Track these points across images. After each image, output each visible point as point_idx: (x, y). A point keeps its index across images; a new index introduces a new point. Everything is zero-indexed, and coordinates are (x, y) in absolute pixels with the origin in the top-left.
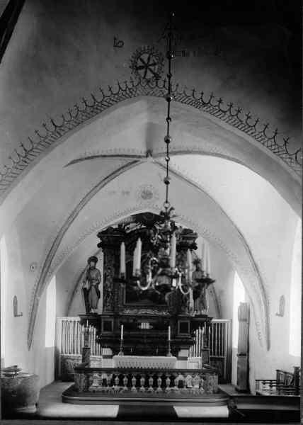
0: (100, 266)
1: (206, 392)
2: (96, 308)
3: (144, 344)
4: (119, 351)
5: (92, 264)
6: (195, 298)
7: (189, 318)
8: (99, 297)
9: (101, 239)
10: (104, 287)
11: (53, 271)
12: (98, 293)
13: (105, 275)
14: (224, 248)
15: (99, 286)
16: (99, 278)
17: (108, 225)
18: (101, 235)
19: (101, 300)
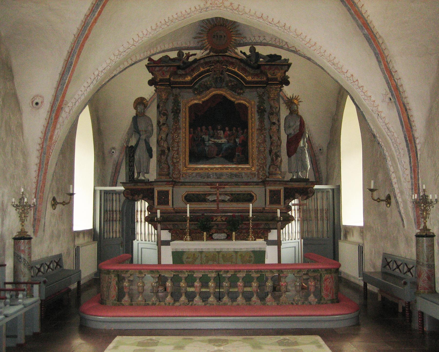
0: (152, 113)
1: (319, 302)
2: (148, 173)
3: (378, 227)
4: (185, 234)
5: (140, 108)
6: (290, 154)
7: (281, 182)
8: (151, 156)
9: (153, 74)
10: (158, 142)
11: (285, 185)
12: (149, 151)
13: (159, 122)
14: (322, 51)
15: (151, 139)
16: (150, 128)
17: (414, 223)
18: (152, 66)
19: (154, 161)
